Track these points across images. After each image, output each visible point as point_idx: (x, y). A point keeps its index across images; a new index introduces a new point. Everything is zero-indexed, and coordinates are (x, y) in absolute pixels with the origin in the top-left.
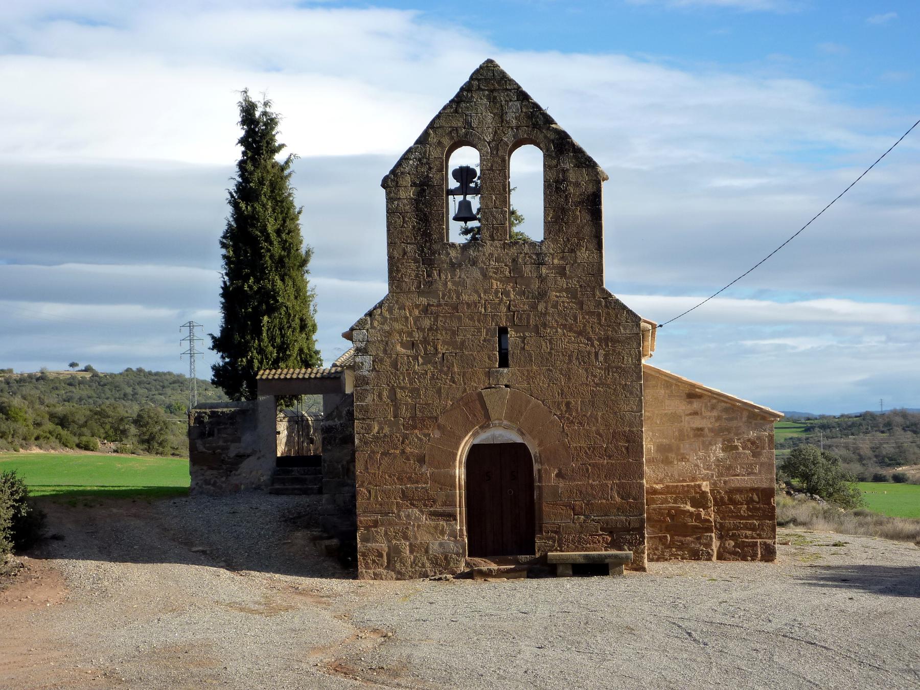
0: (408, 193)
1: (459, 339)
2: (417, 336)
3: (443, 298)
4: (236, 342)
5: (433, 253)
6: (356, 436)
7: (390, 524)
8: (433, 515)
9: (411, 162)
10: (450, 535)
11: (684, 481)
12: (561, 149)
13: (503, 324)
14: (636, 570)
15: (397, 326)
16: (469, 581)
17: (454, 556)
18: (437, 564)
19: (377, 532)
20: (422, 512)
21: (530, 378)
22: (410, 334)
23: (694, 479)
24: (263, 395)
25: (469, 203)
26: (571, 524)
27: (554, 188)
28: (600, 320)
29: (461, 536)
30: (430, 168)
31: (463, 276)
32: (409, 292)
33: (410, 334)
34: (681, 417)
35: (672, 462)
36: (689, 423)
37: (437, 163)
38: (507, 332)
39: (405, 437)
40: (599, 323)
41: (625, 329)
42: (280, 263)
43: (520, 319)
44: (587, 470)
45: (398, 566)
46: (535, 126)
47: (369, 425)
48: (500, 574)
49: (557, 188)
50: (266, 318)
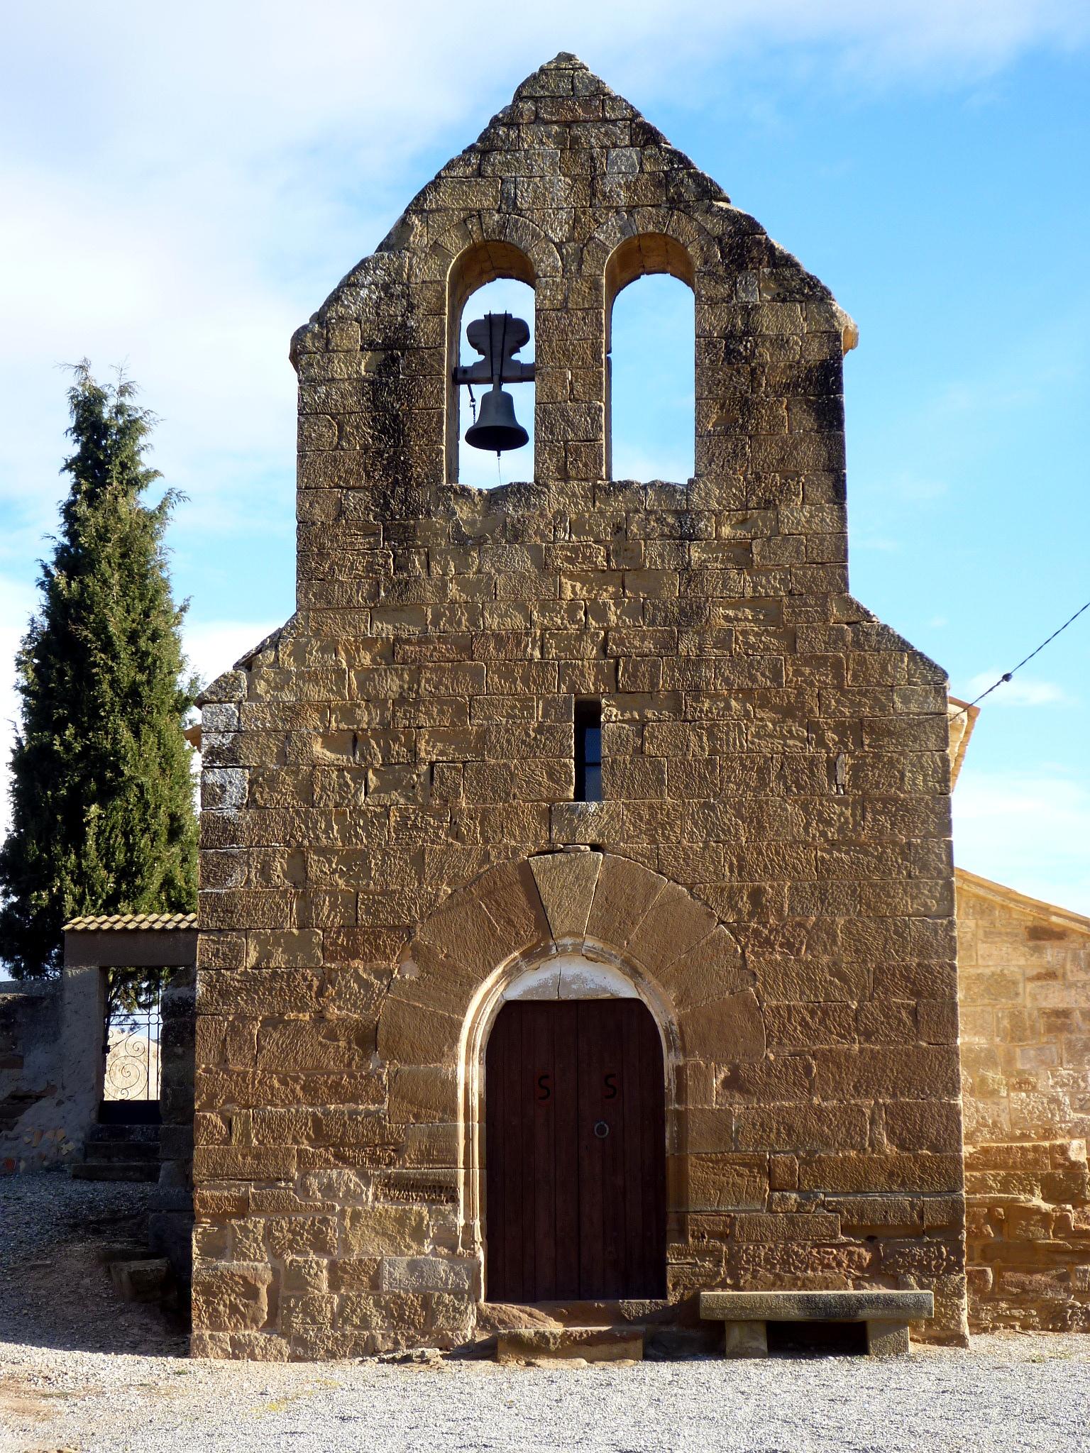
0: (352, 366)
1: (473, 726)
3: (435, 623)
4: (31, 859)
6: (200, 975)
7: (282, 1208)
8: (395, 1186)
9: (364, 293)
10: (437, 1241)
11: (1024, 1137)
12: (737, 261)
13: (589, 685)
14: (940, 1341)
15: (315, 693)
16: (484, 1365)
17: (447, 1298)
18: (401, 1318)
19: (244, 1229)
21: (656, 826)
22: (348, 714)
23: (1048, 1133)
24: (76, 964)
25: (508, 399)
26: (765, 1216)
27: (726, 358)
28: (839, 676)
29: (469, 1242)
30: (411, 307)
31: (487, 567)
32: (350, 607)
33: (348, 714)
34: (1015, 983)
35: (994, 1093)
36: (1034, 998)
37: (429, 294)
38: (597, 709)
40: (839, 687)
41: (906, 700)
42: (133, 696)
43: (633, 676)
44: (808, 1069)
45: (297, 1321)
46: (675, 203)
48: (569, 1348)
49: (729, 352)
50: (94, 809)
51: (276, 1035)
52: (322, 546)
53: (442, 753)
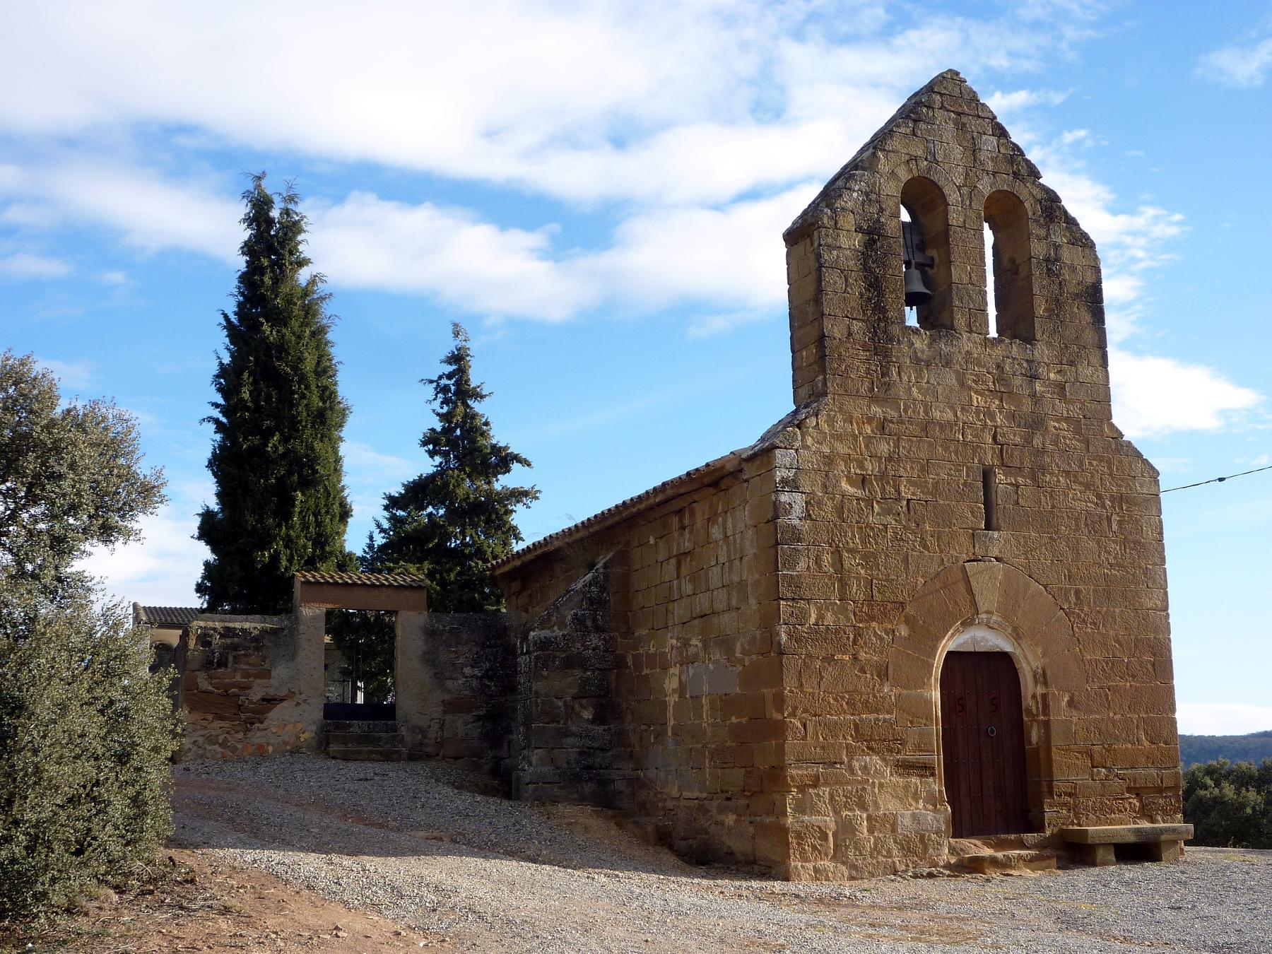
2: (871, 467)
5: (891, 340)
7: (839, 781)
9: (855, 195)
13: (990, 459)
15: (842, 449)
17: (933, 836)
20: (884, 760)
30: (881, 210)
31: (932, 381)
32: (858, 395)
39: (858, 633)
40: (1110, 475)
44: (1107, 695)
47: (802, 610)
51: (830, 669)
52: (840, 355)
53: (913, 494)
